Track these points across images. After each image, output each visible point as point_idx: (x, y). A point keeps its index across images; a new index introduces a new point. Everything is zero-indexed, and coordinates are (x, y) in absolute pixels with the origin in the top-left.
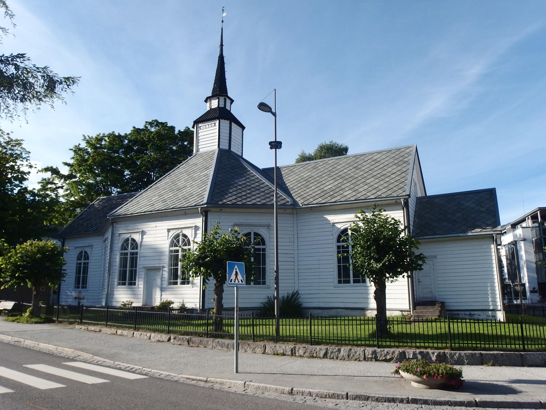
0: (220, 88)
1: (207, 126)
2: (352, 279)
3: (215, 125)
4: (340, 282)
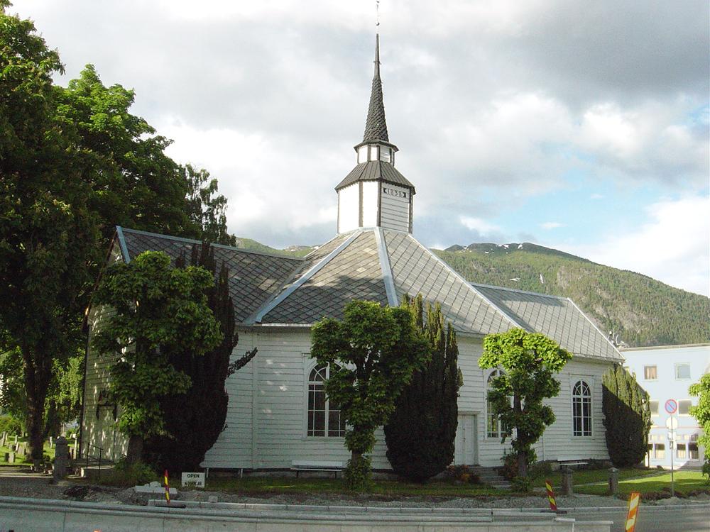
0: (378, 133)
1: (394, 192)
2: (583, 431)
3: (405, 196)
4: (310, 434)
